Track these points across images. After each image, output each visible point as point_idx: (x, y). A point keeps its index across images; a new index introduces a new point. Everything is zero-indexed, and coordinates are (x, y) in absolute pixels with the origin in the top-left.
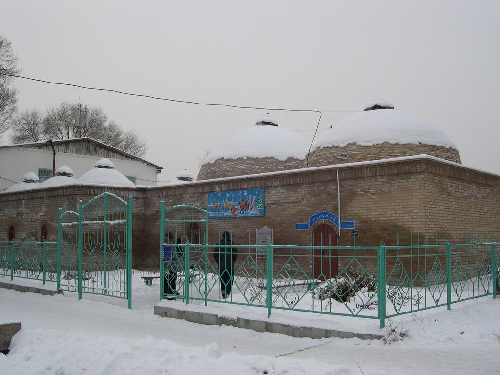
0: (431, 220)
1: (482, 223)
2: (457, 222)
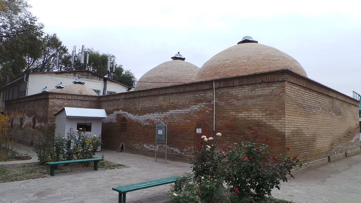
0: (290, 121)
1: (325, 124)
2: (308, 123)
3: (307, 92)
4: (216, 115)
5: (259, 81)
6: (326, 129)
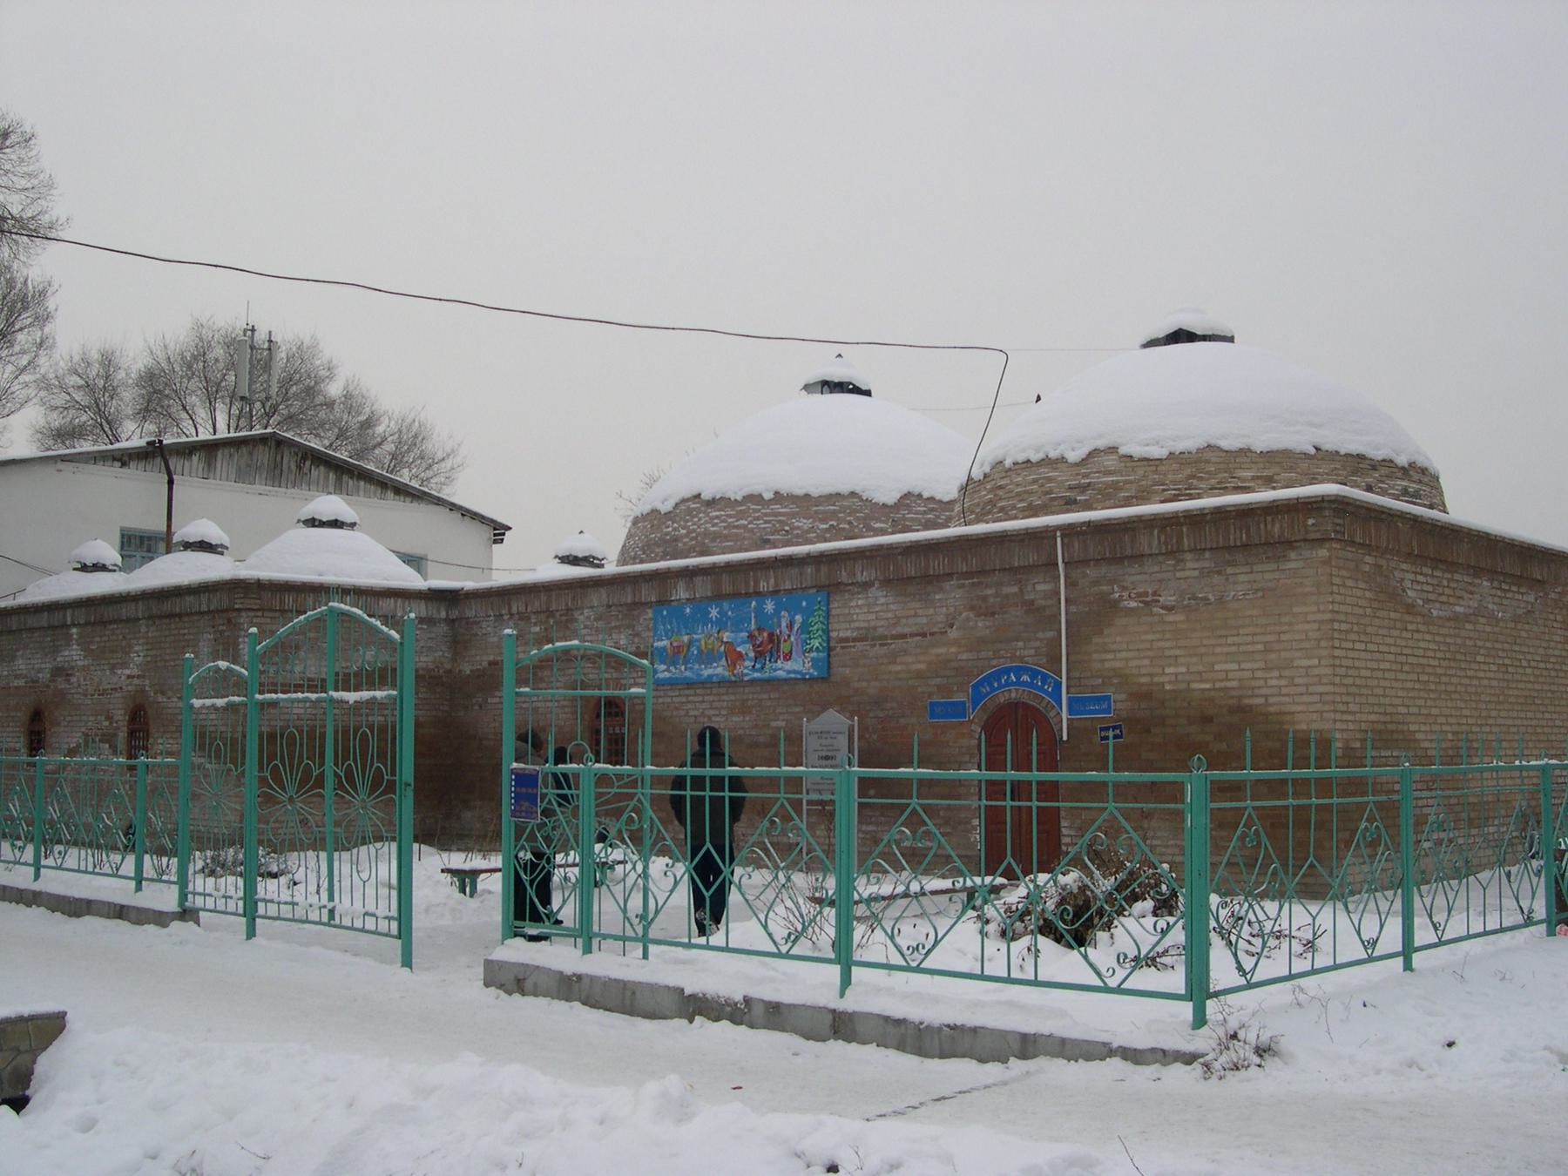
0: (1353, 690)
3: (1426, 575)
4: (1073, 658)
5: (1241, 538)
6: (1518, 722)
